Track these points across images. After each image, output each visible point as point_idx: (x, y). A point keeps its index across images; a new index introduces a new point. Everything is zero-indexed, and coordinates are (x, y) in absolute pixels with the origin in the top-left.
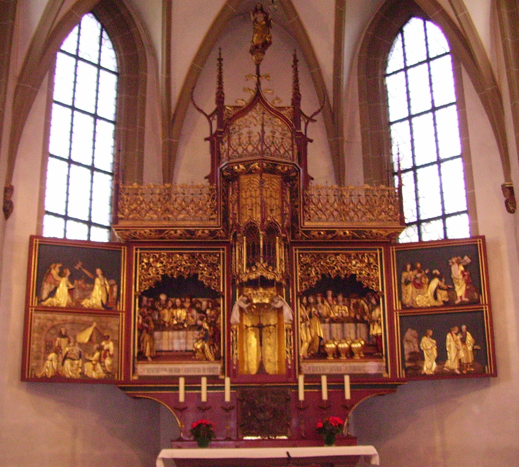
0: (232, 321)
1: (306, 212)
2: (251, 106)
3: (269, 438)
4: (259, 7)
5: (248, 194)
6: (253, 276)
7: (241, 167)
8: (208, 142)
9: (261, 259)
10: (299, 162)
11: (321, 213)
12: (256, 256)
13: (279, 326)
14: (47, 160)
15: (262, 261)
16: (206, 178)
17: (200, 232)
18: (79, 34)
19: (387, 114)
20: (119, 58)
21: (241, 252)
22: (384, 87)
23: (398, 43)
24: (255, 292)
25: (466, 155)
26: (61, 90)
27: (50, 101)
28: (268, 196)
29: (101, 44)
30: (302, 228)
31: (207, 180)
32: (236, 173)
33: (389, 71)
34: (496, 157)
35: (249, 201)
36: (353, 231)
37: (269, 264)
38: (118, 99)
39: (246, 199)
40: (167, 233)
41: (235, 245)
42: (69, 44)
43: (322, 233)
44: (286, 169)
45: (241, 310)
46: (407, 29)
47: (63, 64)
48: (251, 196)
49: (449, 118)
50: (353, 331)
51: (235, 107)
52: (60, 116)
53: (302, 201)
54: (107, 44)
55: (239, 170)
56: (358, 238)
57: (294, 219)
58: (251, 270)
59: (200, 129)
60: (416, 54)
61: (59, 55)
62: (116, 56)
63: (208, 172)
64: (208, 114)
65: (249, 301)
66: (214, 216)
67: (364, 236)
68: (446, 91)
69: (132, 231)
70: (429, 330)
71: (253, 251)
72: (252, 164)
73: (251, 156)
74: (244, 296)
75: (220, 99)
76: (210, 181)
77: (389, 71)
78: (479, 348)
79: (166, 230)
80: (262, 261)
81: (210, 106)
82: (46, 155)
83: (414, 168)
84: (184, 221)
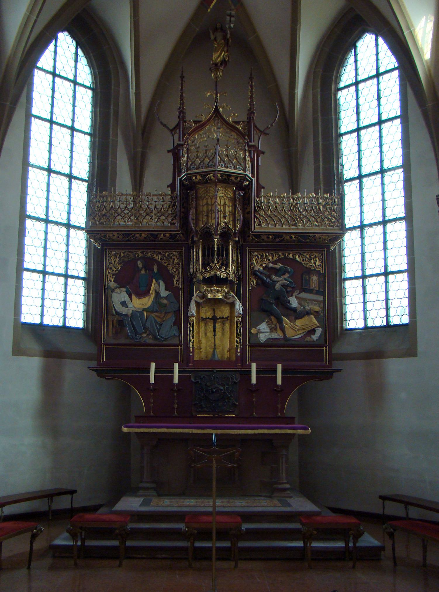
0: (190, 314)
1: (257, 218)
3: (219, 415)
4: (218, 25)
5: (205, 202)
6: (208, 275)
7: (199, 177)
8: (171, 154)
9: (216, 259)
10: (252, 173)
11: (270, 219)
12: (211, 257)
13: (230, 318)
14: (28, 171)
15: (216, 262)
16: (168, 186)
17: (162, 235)
18: (55, 52)
19: (337, 127)
20: (94, 74)
22: (336, 101)
23: (351, 59)
24: (209, 289)
25: (406, 166)
26: (40, 104)
27: (29, 115)
28: (222, 204)
29: (76, 61)
30: (252, 232)
31: (169, 189)
32: (194, 183)
33: (342, 85)
35: (205, 208)
36: (298, 235)
37: (222, 265)
38: (94, 113)
39: (203, 206)
40: (133, 236)
41: (193, 246)
42: (45, 60)
43: (270, 237)
44: (238, 179)
45: (198, 305)
46: (360, 44)
47: (41, 81)
48: (207, 204)
49: (394, 132)
50: (371, 314)
51: (196, 122)
52: (38, 130)
53: (253, 208)
54: (83, 61)
55: (197, 180)
56: (303, 242)
57: (247, 224)
58: (206, 269)
60: (367, 68)
61: (36, 72)
62: (91, 72)
63: (170, 181)
64: (171, 128)
65: (204, 297)
66: (174, 221)
67: (308, 240)
68: (392, 105)
69: (102, 235)
72: (207, 175)
73: (207, 167)
74: (200, 292)
75: (182, 113)
76: (171, 190)
79: (132, 233)
80: (216, 262)
81: (173, 122)
82: (26, 164)
83: (360, 177)
84: (150, 224)
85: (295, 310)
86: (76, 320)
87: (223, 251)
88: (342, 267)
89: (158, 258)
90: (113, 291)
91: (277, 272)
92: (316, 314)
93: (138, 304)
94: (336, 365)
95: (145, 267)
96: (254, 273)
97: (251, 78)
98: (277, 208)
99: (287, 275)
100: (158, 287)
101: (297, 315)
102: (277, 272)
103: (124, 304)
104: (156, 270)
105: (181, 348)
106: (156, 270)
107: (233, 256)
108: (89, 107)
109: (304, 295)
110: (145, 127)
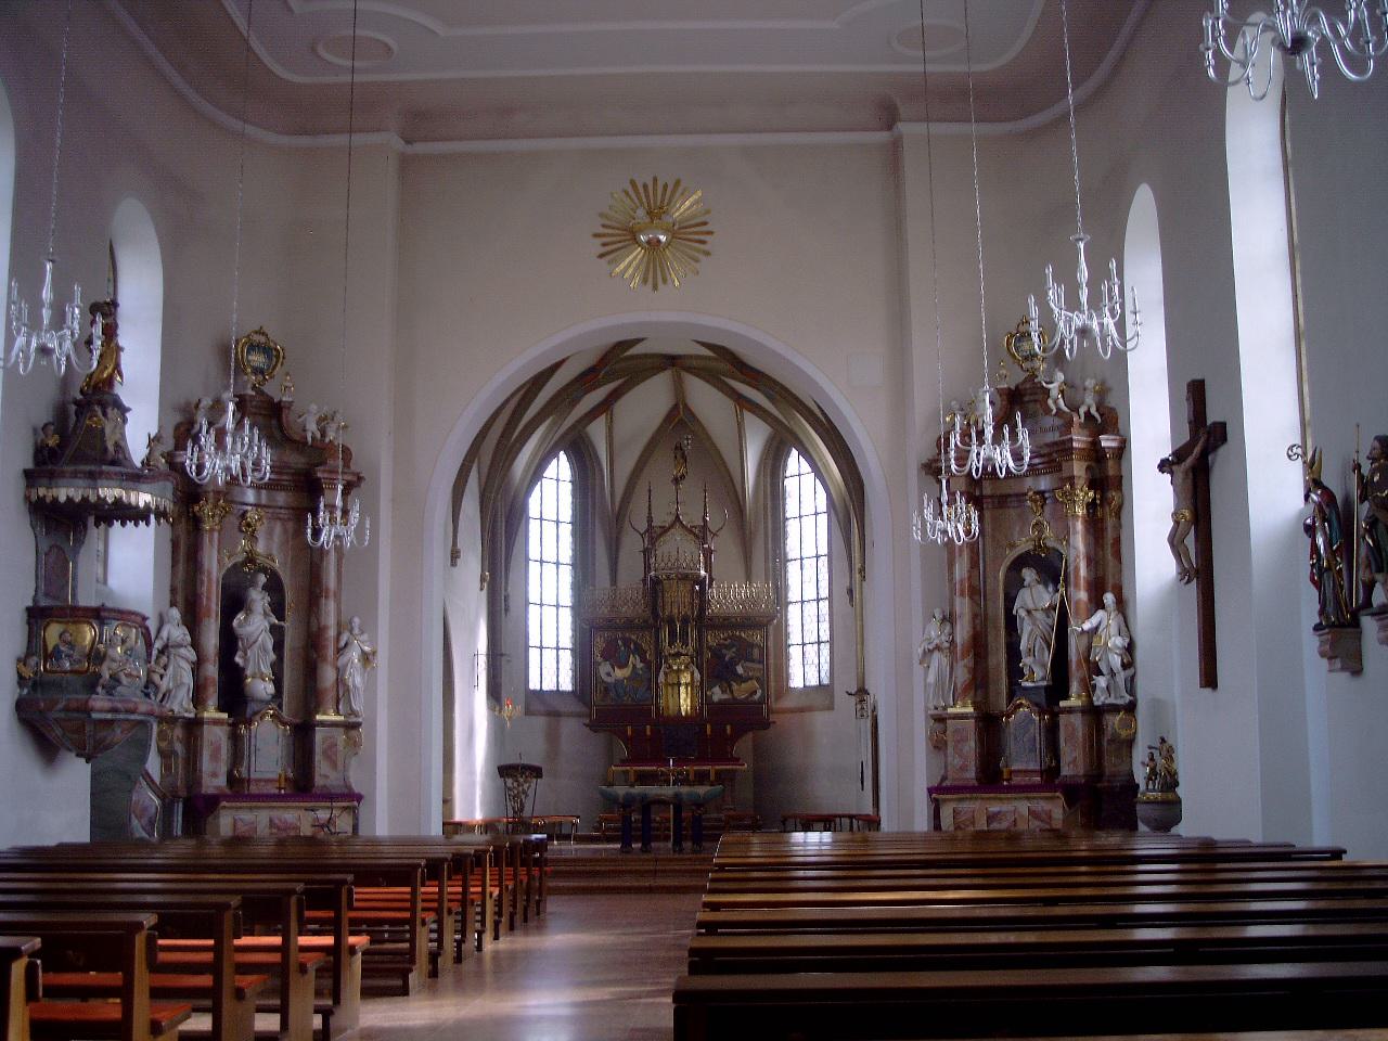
2: (672, 526)
21: (665, 634)
34: (846, 564)
45: (666, 674)
50: (808, 676)
57: (702, 610)
59: (632, 545)
70: (211, 977)
71: (672, 634)
75: (650, 520)
77: (788, 474)
78: (798, 836)
81: (643, 527)
85: (740, 676)
86: (567, 685)
87: (684, 634)
88: (787, 635)
89: (633, 637)
90: (600, 664)
91: (726, 647)
92: (758, 680)
93: (619, 673)
94: (773, 718)
95: (624, 645)
96: (709, 648)
97: (705, 491)
98: (730, 593)
99: (734, 650)
100: (634, 660)
101: (742, 679)
102: (726, 647)
103: (609, 674)
104: (632, 646)
105: (653, 708)
106: (632, 646)
107: (693, 634)
108: (570, 499)
109: (749, 664)
110: (619, 513)
